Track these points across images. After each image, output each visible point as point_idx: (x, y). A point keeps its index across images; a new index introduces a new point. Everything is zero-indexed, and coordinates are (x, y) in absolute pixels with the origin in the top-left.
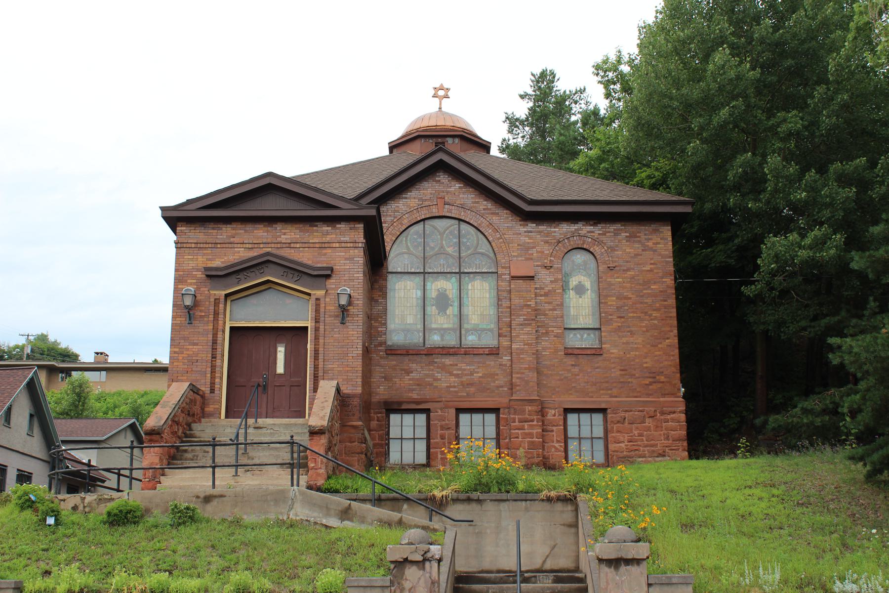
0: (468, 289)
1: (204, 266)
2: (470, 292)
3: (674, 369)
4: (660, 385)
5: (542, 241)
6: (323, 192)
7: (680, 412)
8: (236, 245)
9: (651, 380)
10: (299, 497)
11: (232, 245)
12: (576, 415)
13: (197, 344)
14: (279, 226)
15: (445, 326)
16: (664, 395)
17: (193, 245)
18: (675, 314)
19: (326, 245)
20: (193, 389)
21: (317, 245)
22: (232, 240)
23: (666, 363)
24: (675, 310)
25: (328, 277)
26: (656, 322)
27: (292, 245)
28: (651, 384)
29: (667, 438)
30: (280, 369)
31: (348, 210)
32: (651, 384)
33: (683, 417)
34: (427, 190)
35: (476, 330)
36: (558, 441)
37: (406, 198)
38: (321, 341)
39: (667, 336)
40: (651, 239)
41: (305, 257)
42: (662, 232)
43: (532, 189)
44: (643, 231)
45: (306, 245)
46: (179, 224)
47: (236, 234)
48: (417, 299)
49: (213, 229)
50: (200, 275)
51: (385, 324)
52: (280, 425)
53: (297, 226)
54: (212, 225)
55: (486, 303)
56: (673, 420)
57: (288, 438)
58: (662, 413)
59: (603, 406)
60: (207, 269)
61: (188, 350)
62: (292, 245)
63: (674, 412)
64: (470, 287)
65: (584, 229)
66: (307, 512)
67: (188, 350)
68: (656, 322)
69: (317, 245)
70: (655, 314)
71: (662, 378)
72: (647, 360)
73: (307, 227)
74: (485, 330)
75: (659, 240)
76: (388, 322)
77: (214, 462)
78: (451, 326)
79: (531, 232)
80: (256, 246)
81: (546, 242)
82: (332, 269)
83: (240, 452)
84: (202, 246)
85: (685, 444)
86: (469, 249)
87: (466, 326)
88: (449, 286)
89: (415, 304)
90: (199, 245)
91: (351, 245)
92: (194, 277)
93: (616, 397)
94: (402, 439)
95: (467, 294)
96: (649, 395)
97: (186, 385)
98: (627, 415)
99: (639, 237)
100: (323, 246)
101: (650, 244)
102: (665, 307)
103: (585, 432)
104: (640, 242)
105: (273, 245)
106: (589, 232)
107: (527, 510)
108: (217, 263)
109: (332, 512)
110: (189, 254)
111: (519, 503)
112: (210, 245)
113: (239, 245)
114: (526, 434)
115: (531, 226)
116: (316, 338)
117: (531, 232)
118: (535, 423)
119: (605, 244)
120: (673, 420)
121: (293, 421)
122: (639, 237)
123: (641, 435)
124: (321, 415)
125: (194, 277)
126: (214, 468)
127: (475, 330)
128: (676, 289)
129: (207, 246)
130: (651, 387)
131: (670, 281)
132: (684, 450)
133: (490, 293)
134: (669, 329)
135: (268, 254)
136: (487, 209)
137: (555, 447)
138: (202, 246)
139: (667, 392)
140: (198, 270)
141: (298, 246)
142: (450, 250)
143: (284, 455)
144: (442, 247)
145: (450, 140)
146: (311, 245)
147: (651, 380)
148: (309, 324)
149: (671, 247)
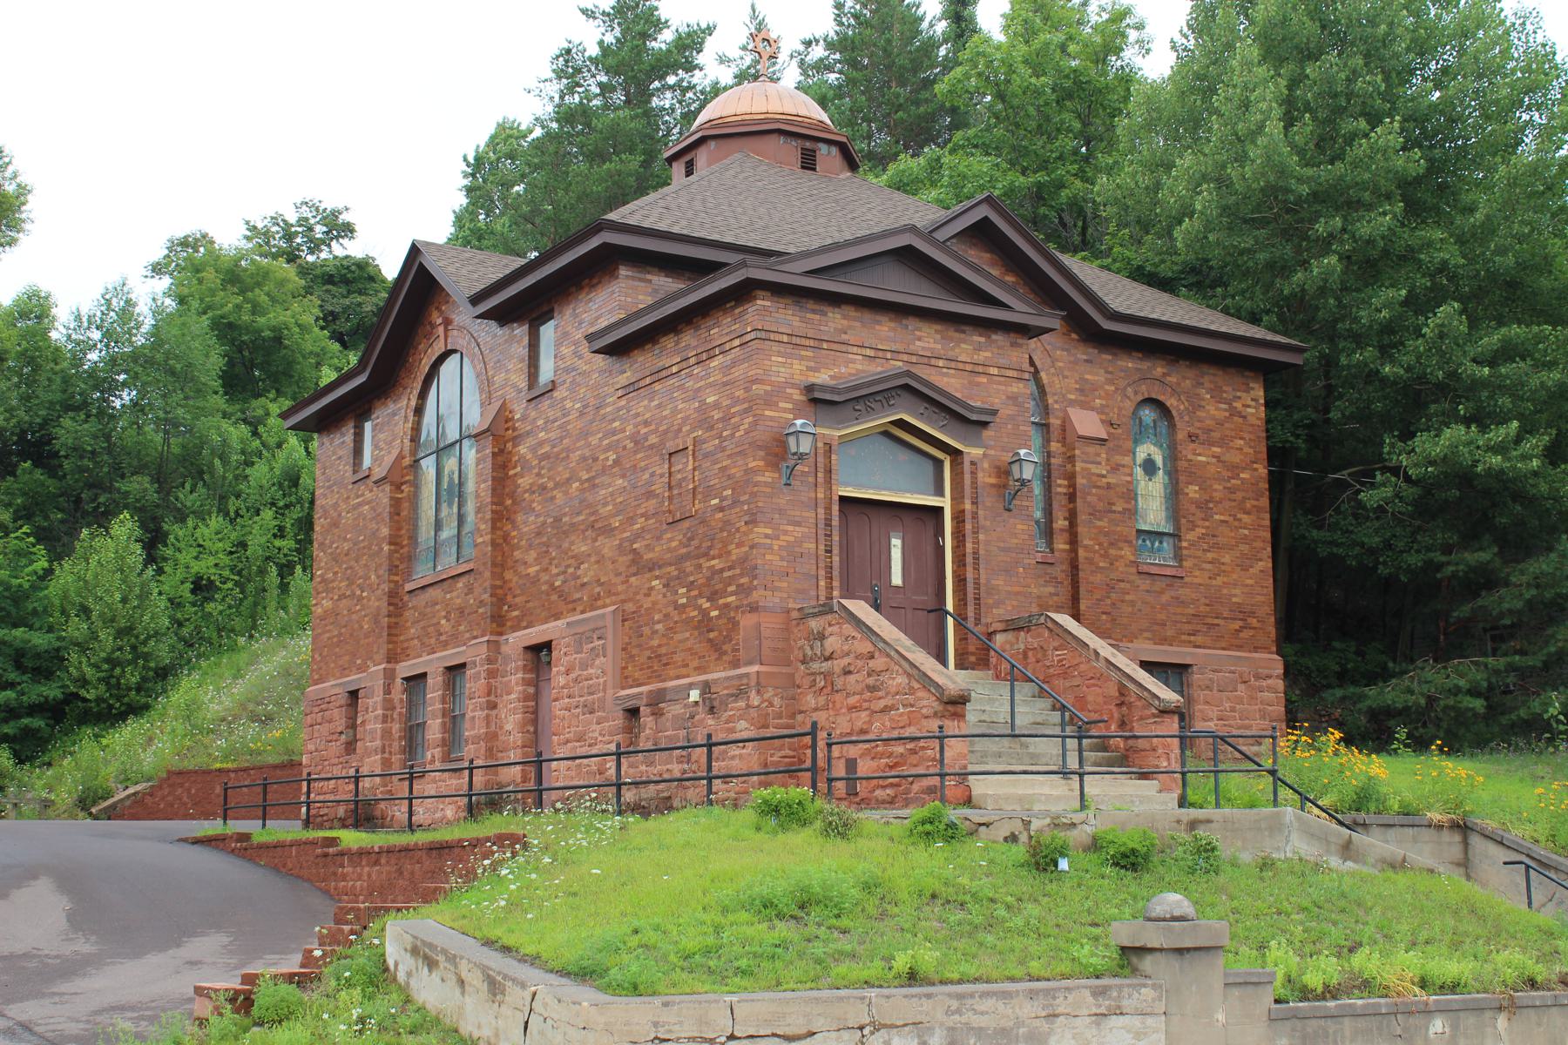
4: (1251, 632)
6: (836, 246)
8: (851, 349)
10: (1296, 824)
11: (844, 348)
13: (798, 524)
14: (912, 323)
17: (785, 339)
18: (1268, 523)
19: (980, 369)
21: (969, 367)
22: (844, 337)
24: (1268, 516)
25: (985, 424)
27: (933, 362)
30: (897, 580)
33: (1280, 685)
41: (950, 383)
44: (1227, 383)
45: (953, 365)
46: (760, 293)
47: (850, 327)
49: (814, 311)
50: (797, 395)
53: (938, 327)
54: (811, 305)
58: (1258, 677)
60: (810, 388)
61: (786, 533)
62: (933, 362)
67: (786, 533)
69: (969, 367)
70: (1246, 518)
72: (1237, 591)
73: (951, 333)
80: (880, 354)
84: (798, 341)
90: (794, 340)
91: (1015, 374)
92: (789, 399)
96: (1239, 647)
98: (1215, 676)
100: (976, 370)
101: (1238, 405)
105: (905, 357)
107: (1415, 840)
108: (822, 378)
109: (1333, 848)
110: (779, 354)
111: (1406, 829)
112: (812, 343)
113: (855, 350)
123: (1233, 710)
125: (789, 399)
126: (1081, 775)
128: (1270, 482)
129: (807, 342)
131: (1262, 470)
135: (908, 374)
138: (798, 341)
140: (794, 386)
141: (941, 363)
145: (823, 148)
146: (961, 366)
148: (945, 502)
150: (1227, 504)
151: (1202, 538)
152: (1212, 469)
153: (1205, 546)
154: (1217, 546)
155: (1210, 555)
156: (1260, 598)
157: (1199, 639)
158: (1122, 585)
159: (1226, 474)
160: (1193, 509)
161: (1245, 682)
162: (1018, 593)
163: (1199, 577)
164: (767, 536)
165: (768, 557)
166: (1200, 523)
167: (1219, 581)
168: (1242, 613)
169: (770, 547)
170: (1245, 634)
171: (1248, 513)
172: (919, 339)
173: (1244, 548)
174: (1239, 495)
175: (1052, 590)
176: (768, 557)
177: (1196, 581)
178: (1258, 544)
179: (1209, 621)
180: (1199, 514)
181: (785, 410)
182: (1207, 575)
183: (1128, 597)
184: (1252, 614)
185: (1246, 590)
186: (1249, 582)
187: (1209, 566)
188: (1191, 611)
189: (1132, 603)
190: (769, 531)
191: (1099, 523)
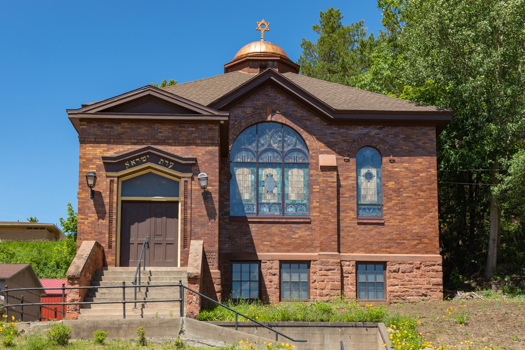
0: (288, 175)
1: (102, 155)
2: (290, 177)
3: (434, 234)
4: (424, 245)
5: (342, 140)
7: (438, 265)
9: (418, 241)
12: (239, 265)
15: (272, 201)
16: (427, 253)
18: (436, 195)
20: (97, 245)
23: (429, 230)
26: (423, 200)
28: (418, 244)
29: (429, 283)
31: (207, 115)
32: (418, 244)
34: (259, 100)
35: (293, 204)
36: (352, 284)
37: (244, 107)
38: (189, 211)
39: (430, 210)
40: (421, 140)
42: (429, 135)
43: (335, 102)
48: (252, 181)
50: (100, 162)
51: (229, 199)
52: (161, 272)
55: (302, 185)
56: (433, 271)
57: (177, 282)
59: (384, 260)
60: (104, 158)
63: (434, 265)
64: (290, 173)
65: (373, 131)
66: (192, 335)
67: (91, 217)
68: (423, 200)
70: (422, 194)
71: (426, 241)
72: (416, 227)
74: (300, 204)
75: (427, 141)
76: (231, 198)
77: (124, 298)
78: (276, 201)
79: (334, 133)
81: (345, 141)
82: (195, 160)
83: (137, 291)
85: (441, 287)
86: (289, 145)
87: (287, 201)
88: (275, 173)
89: (250, 185)
93: (393, 253)
94: (241, 281)
95: (287, 178)
97: (94, 242)
99: (413, 138)
101: (420, 143)
102: (430, 189)
103: (245, 277)
104: (413, 142)
106: (376, 134)
107: (342, 334)
108: (111, 153)
114: (330, 279)
115: (335, 129)
116: (185, 210)
117: (334, 133)
118: (336, 271)
119: (387, 143)
120: (433, 271)
121: (169, 269)
122: (413, 138)
124: (195, 265)
126: (124, 303)
127: (293, 204)
130: (418, 247)
132: (441, 291)
133: (304, 178)
134: (432, 205)
135: (149, 148)
136: (303, 116)
137: (349, 288)
139: (429, 250)
142: (275, 146)
143: (153, 294)
144: (270, 145)
147: (418, 241)
149: (435, 146)
150: (411, 189)
151: (396, 205)
152: (403, 174)
153: (398, 208)
154: (405, 208)
155: (400, 212)
156: (429, 230)
157: (392, 250)
158: (348, 229)
159: (411, 175)
160: (391, 192)
161: (420, 267)
162: (208, 234)
163: (393, 222)
164: (82, 219)
165: (82, 227)
166: (395, 198)
167: (405, 223)
168: (419, 237)
169: (83, 223)
170: (420, 246)
171: (425, 191)
172: (161, 133)
173: (422, 208)
174: (419, 184)
175: (309, 233)
176: (82, 227)
177: (391, 224)
178: (430, 205)
179: (399, 241)
180: (394, 194)
181: (92, 168)
182: (397, 221)
183: (351, 234)
184: (425, 237)
185: (421, 226)
186: (424, 222)
187: (399, 217)
188: (388, 237)
189: (353, 236)
190: (83, 217)
191: (332, 203)
